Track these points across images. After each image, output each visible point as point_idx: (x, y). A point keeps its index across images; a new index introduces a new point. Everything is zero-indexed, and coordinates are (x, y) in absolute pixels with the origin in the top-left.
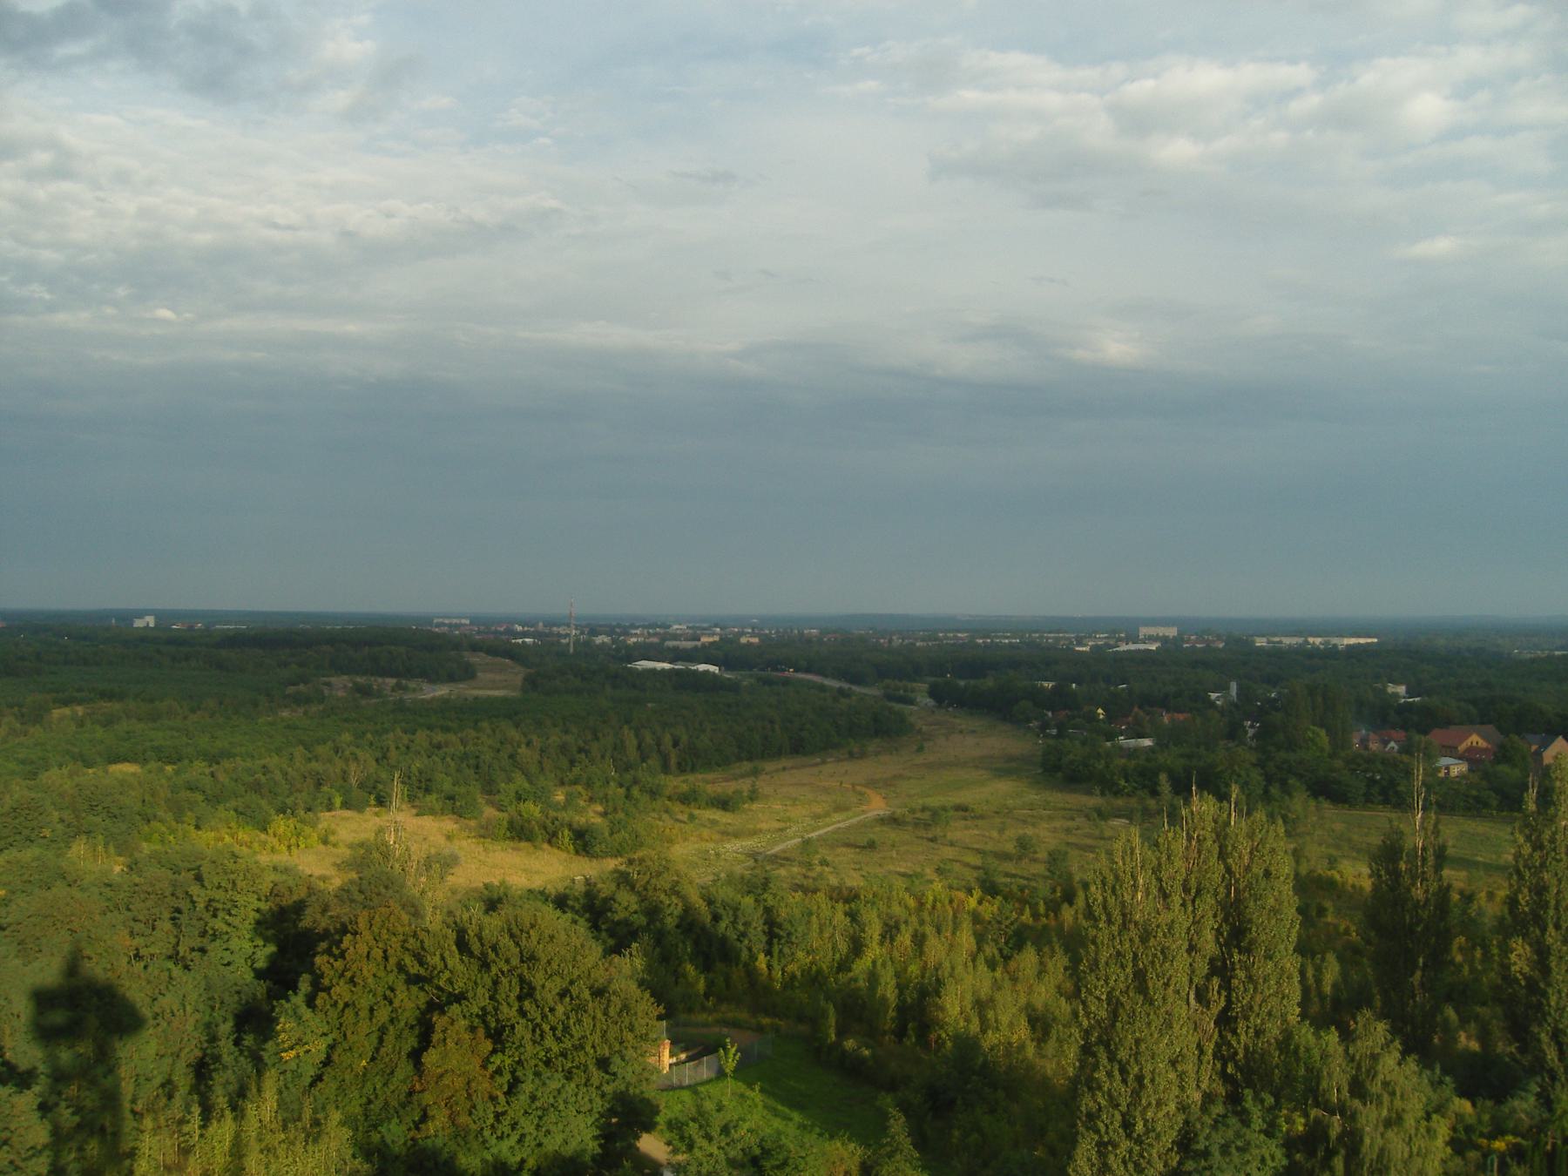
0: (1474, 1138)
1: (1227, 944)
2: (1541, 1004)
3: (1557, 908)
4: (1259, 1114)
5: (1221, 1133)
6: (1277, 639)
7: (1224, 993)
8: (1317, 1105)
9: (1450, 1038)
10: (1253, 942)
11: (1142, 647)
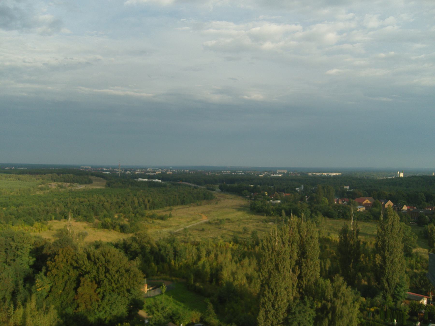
1: (301, 256)
3: (388, 246)
4: (309, 302)
6: (314, 173)
7: (300, 270)
8: (324, 300)
11: (278, 175)
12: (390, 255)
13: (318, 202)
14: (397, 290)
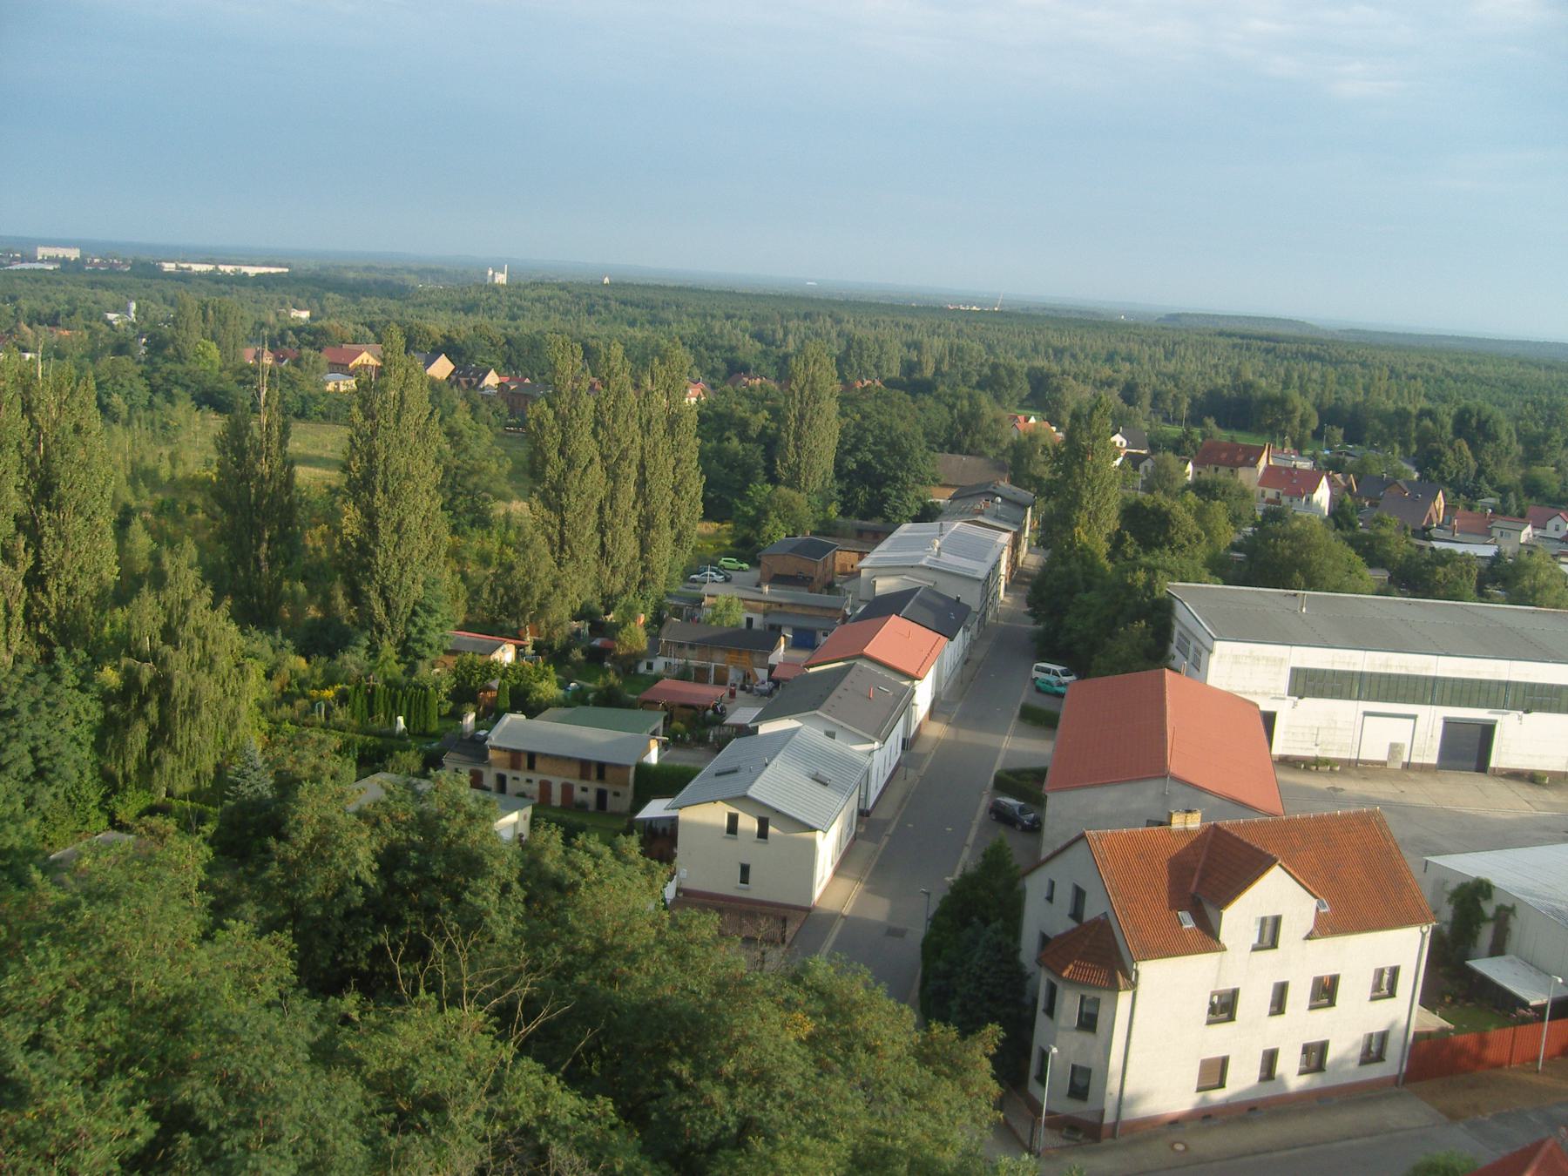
0: (306, 689)
1: (35, 502)
2: (370, 563)
3: (384, 473)
4: (71, 669)
5: (29, 691)
6: (185, 266)
7: (31, 551)
8: (130, 654)
9: (298, 613)
10: (60, 498)
11: (37, 266)
12: (392, 505)
13: (180, 357)
14: (415, 625)
